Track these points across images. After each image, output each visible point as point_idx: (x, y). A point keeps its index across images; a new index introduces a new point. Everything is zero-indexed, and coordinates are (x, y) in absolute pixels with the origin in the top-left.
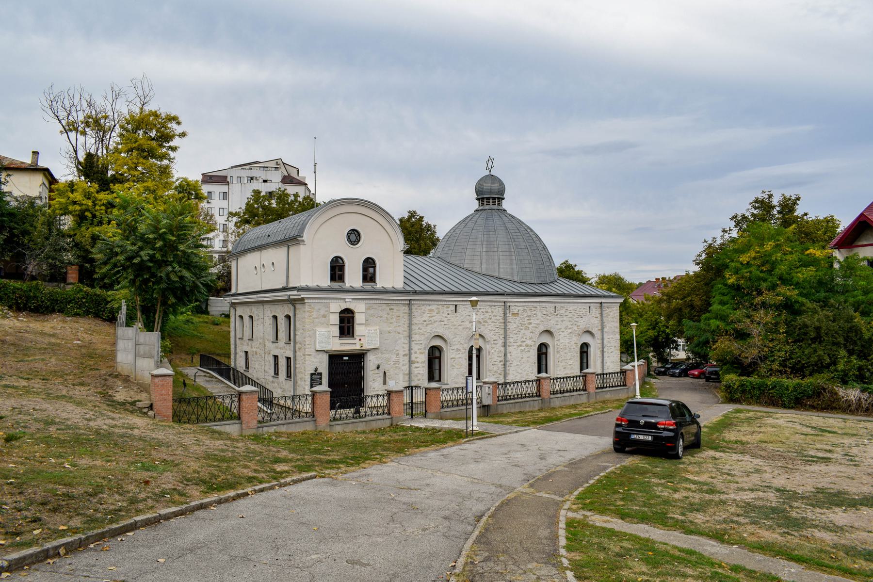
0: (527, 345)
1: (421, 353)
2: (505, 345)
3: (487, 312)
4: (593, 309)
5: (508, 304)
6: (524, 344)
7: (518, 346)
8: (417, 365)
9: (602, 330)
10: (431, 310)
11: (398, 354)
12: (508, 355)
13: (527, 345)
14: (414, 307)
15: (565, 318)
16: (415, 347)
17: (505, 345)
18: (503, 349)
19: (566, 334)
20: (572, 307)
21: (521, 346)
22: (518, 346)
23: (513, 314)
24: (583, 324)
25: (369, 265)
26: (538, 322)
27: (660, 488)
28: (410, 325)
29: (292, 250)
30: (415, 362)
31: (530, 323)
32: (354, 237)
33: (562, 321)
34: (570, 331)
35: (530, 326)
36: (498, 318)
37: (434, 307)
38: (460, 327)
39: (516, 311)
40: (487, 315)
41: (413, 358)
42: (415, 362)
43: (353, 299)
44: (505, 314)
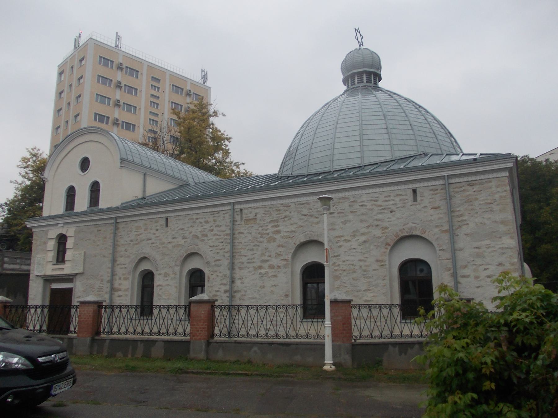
0: (271, 267)
1: (125, 279)
2: (232, 267)
3: (207, 222)
4: (426, 197)
5: (238, 207)
6: (266, 265)
7: (255, 269)
8: (120, 293)
9: (452, 233)
10: (138, 228)
11: (102, 280)
12: (238, 283)
13: (271, 267)
14: (120, 226)
15: (351, 217)
16: (119, 271)
17: (232, 267)
18: (228, 273)
19: (354, 244)
20: (364, 196)
21: (260, 267)
22: (255, 269)
23: (247, 220)
24: (397, 224)
25: (95, 188)
26: (292, 228)
27: (519, 300)
28: (115, 245)
29: (140, 196)
30: (119, 290)
31: (278, 232)
32: (85, 164)
33: (344, 223)
34: (363, 238)
35: (278, 237)
36: (223, 228)
37: (141, 223)
38: (170, 246)
39: (251, 216)
40: (207, 226)
41: (116, 285)
42: (119, 290)
43: (64, 223)
44: (234, 221)
